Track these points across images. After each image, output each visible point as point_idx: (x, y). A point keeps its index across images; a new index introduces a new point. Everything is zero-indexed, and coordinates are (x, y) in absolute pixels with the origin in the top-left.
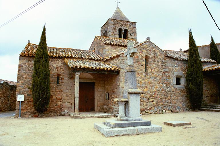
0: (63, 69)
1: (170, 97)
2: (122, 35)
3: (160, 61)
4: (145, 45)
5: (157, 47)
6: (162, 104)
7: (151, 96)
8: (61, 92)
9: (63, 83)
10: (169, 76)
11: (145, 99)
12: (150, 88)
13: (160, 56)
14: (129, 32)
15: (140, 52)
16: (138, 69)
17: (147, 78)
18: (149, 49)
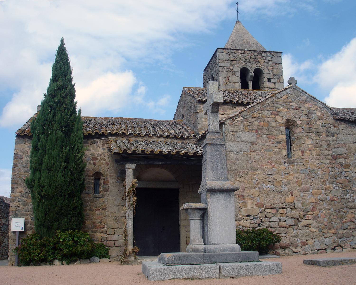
0: (107, 160)
1: (353, 215)
2: (250, 84)
3: (323, 130)
4: (284, 97)
5: (315, 98)
6: (333, 231)
7: (304, 213)
8: (103, 211)
9: (106, 190)
10: (347, 166)
11: (291, 222)
12: (302, 194)
13: (322, 119)
14: (266, 74)
15: (272, 114)
16: (269, 150)
18: (294, 105)
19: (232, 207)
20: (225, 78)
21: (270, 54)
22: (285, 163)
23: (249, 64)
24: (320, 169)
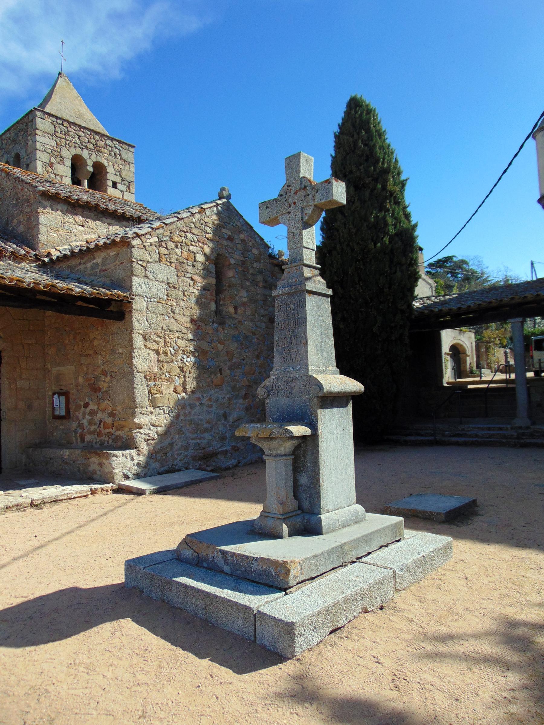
17: (221, 336)
19: (349, 430)
20: (46, 164)
21: (118, 143)
22: (213, 322)
23: (85, 151)
24: (254, 337)
